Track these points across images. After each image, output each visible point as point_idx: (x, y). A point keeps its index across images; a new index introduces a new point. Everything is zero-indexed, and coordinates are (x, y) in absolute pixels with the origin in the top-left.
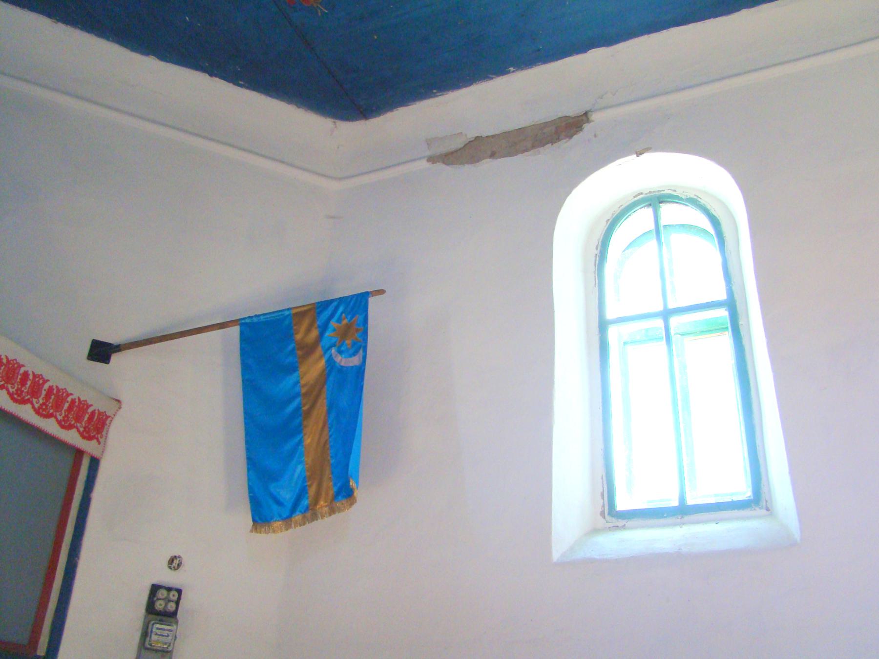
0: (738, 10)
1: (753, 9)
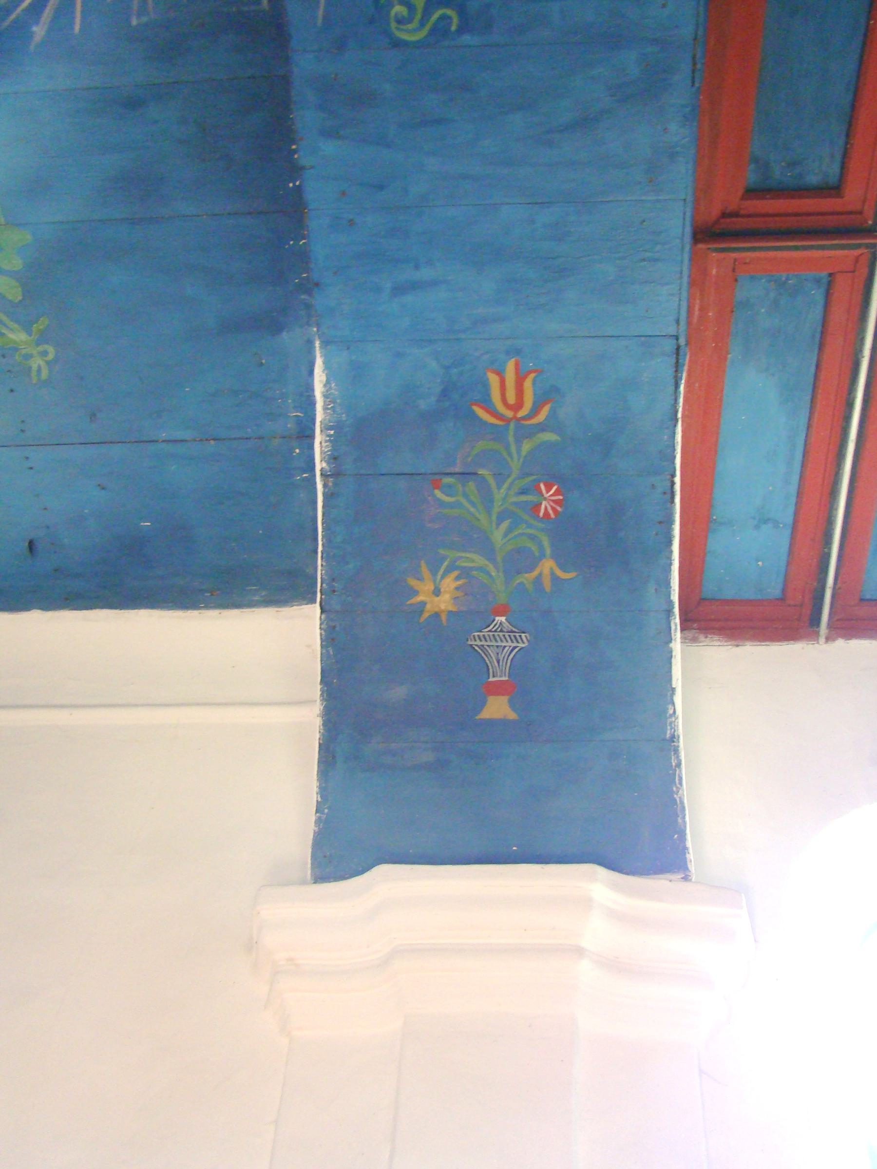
0: (29, 610)
1: (50, 614)
